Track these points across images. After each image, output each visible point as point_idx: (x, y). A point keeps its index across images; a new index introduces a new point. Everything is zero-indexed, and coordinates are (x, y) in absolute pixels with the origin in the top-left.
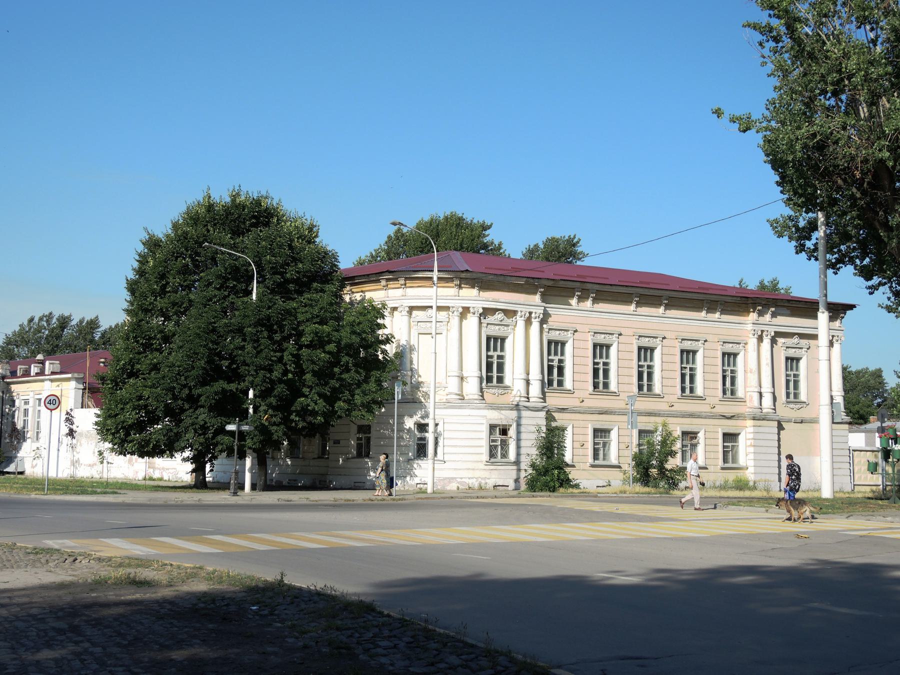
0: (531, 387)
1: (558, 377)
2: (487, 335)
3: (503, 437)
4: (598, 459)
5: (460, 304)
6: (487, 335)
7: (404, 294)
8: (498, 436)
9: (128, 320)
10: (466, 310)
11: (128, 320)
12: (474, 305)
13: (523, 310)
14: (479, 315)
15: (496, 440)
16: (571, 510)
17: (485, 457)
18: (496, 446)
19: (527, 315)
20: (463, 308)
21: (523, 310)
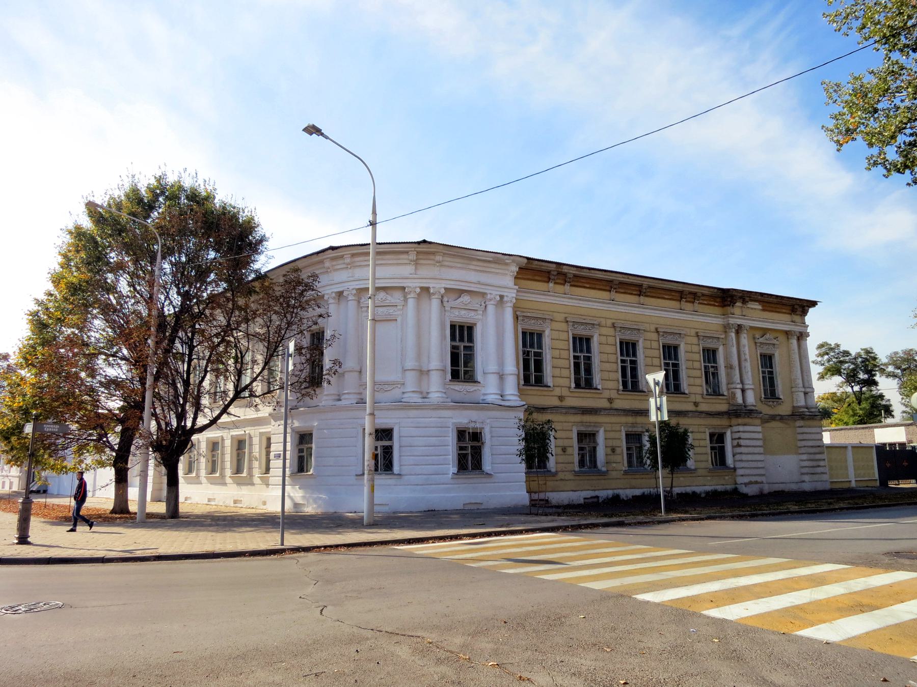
0: (743, 452)
1: (674, 381)
2: (457, 428)
3: (475, 444)
4: (584, 466)
5: (414, 284)
6: (457, 428)
7: (350, 275)
8: (469, 444)
9: (273, 350)
10: (425, 290)
11: (273, 350)
12: (434, 285)
13: (494, 294)
14: (440, 297)
15: (466, 447)
16: (571, 551)
17: (453, 469)
18: (465, 455)
19: (498, 298)
20: (421, 288)
21: (494, 294)
